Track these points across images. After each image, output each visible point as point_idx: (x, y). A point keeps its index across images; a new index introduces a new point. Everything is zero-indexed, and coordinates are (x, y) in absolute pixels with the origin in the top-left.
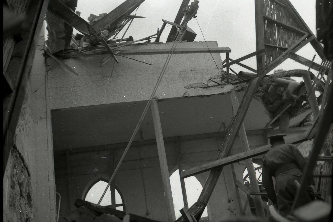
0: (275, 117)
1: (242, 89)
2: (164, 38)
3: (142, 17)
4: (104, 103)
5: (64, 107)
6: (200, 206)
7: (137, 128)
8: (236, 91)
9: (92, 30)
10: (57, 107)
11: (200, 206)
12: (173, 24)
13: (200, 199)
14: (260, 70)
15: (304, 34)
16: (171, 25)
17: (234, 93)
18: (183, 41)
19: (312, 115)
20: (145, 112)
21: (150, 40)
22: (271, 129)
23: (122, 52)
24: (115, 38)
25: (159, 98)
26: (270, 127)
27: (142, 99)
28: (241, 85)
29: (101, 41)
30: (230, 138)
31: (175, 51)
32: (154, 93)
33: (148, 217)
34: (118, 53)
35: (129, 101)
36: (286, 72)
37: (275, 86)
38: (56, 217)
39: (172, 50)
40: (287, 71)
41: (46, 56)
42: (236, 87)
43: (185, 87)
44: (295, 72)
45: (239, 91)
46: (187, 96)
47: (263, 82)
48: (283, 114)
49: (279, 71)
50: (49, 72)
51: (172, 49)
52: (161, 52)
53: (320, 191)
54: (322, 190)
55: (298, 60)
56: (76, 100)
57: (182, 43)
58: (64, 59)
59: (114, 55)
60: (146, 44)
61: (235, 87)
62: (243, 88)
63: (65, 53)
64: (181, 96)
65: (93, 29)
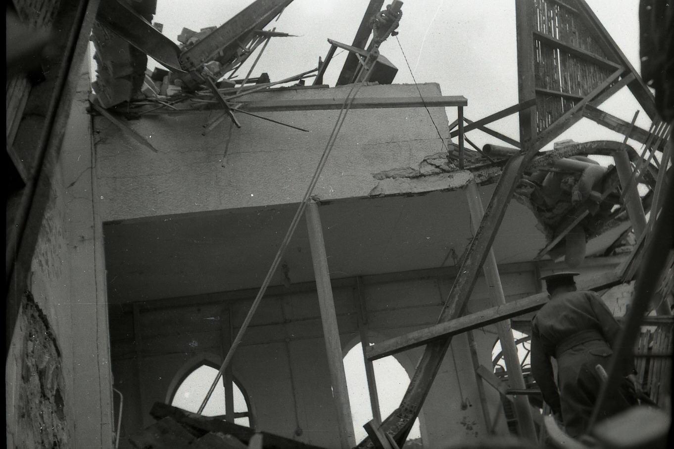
0: (557, 236)
1: (490, 181)
2: (331, 77)
3: (287, 35)
4: (211, 208)
5: (129, 217)
6: (406, 417)
7: (278, 260)
8: (477, 184)
9: (187, 61)
10: (116, 216)
11: (405, 417)
12: (349, 48)
13: (405, 403)
14: (526, 141)
15: (614, 70)
16: (346, 51)
17: (473, 188)
18: (371, 83)
19: (632, 232)
20: (293, 227)
21: (304, 81)
22: (548, 260)
23: (247, 105)
24: (232, 77)
25: (322, 199)
26: (547, 257)
27: (288, 200)
28: (488, 173)
29: (204, 83)
30: (465, 279)
31: (355, 102)
32: (311, 188)
33: (300, 439)
34: (239, 108)
35: (260, 205)
36: (578, 145)
37: (556, 173)
38: (114, 440)
39: (349, 102)
40: (581, 144)
41: (94, 114)
42: (477, 175)
43: (374, 177)
44: (596, 145)
45: (483, 184)
46: (378, 194)
47: (533, 165)
48: (573, 230)
49: (564, 143)
50: (99, 146)
51: (347, 99)
52: (325, 105)
53: (648, 386)
54: (651, 384)
55: (603, 121)
56: (155, 203)
57: (368, 87)
58: (129, 120)
59: (231, 112)
60: (296, 90)
61: (475, 176)
62: (491, 178)
63: (132, 108)
64: (366, 195)
65: (188, 59)
